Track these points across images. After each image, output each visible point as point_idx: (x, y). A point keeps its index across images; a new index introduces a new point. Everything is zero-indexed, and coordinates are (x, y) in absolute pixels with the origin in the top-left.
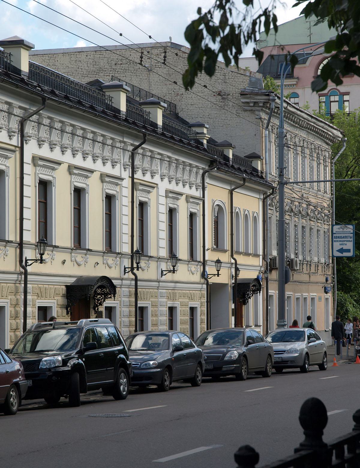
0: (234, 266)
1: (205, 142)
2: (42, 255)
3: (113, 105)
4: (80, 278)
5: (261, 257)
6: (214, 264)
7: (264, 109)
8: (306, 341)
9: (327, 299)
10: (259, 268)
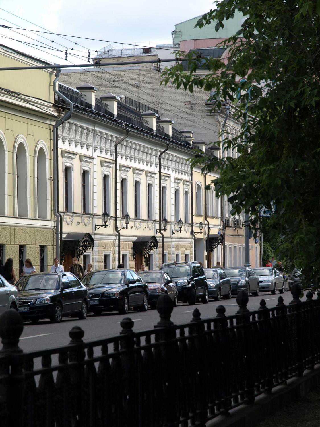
0: (207, 226)
1: (191, 143)
2: (105, 222)
3: (149, 126)
4: (139, 237)
5: (220, 219)
6: (198, 225)
7: (221, 114)
8: (274, 275)
9: (256, 247)
10: (219, 227)
